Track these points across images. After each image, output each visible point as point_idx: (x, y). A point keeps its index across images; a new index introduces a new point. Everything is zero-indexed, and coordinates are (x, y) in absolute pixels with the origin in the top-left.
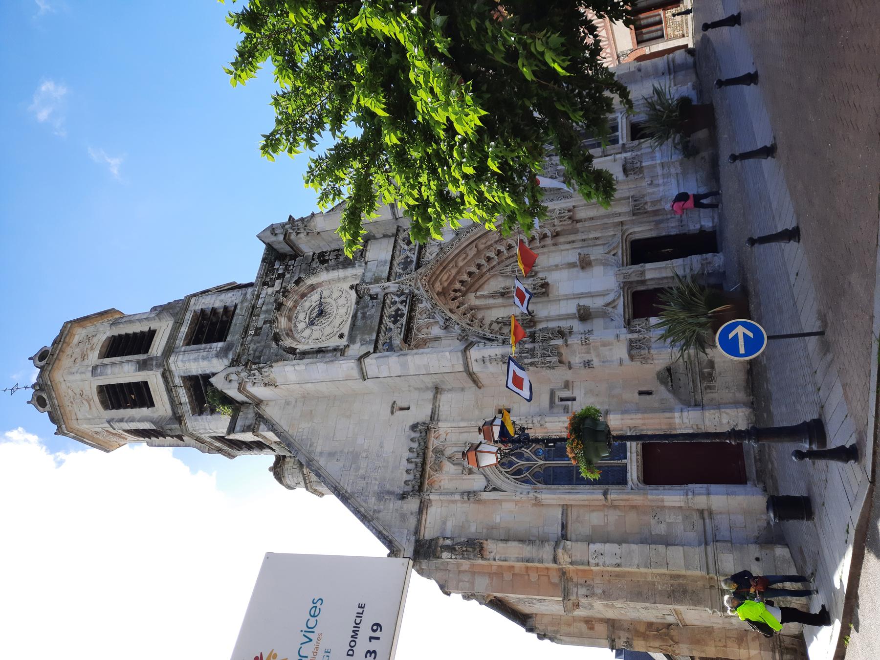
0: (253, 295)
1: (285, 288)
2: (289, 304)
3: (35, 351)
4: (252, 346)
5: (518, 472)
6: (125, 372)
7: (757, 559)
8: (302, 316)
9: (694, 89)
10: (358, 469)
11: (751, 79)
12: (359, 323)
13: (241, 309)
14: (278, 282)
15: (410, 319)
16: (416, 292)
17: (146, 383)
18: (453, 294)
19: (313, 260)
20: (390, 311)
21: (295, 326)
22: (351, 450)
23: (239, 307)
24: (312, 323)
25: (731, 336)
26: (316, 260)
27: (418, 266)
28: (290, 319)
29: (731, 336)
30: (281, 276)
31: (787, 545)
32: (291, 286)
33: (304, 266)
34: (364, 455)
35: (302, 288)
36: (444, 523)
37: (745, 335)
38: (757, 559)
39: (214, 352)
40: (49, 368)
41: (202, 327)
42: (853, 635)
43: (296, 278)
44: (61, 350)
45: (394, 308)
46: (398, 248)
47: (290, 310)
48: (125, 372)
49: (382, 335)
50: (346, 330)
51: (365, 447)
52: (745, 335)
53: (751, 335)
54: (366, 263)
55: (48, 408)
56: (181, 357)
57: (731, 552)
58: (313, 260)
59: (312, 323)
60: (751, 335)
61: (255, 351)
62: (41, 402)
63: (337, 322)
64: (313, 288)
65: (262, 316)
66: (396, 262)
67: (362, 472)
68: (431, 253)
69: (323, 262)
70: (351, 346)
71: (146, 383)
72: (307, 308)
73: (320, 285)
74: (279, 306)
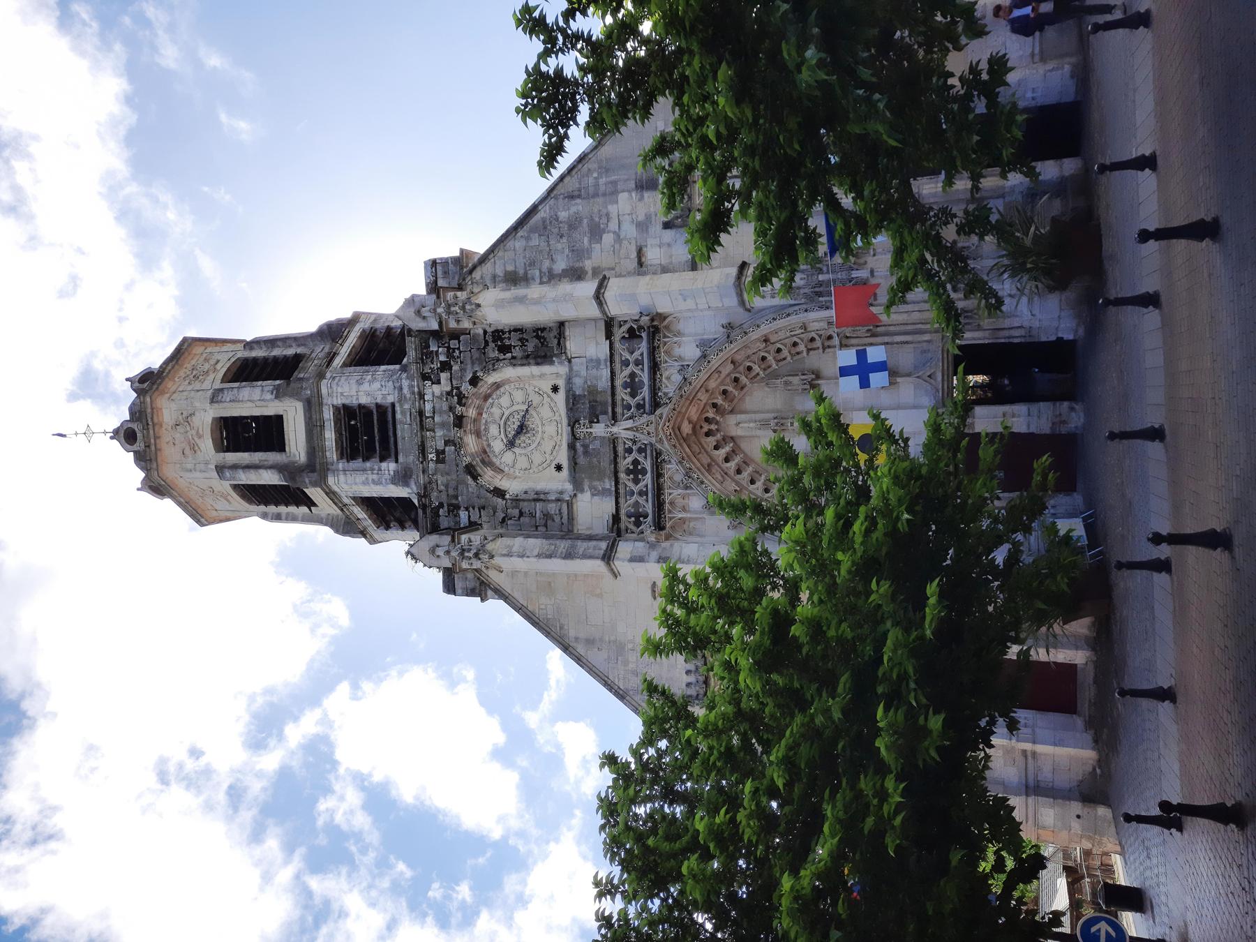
0: (413, 393)
1: (458, 388)
2: (471, 413)
3: (137, 369)
4: (441, 479)
6: (255, 401)
7: (1078, 817)
8: (494, 430)
9: (1072, 77)
10: (626, 663)
11: (1165, 695)
12: (582, 460)
13: (403, 413)
14: (444, 376)
15: (658, 475)
16: (659, 446)
17: (279, 419)
18: (706, 427)
19: (487, 343)
20: (626, 462)
21: (489, 445)
22: (612, 638)
23: (398, 408)
24: (511, 444)
25: (1093, 930)
26: (492, 345)
27: (656, 405)
28: (478, 434)
29: (1093, 930)
30: (445, 367)
31: (1109, 806)
32: (466, 388)
33: (476, 355)
34: (630, 646)
35: (483, 388)
37: (1107, 933)
38: (1078, 817)
39: (387, 476)
40: (154, 466)
41: (353, 431)
42: (1156, 829)
43: (469, 376)
44: (156, 438)
45: (630, 459)
47: (475, 420)
48: (255, 401)
49: (622, 500)
50: (563, 457)
51: (630, 637)
52: (1107, 933)
53: (1113, 934)
54: (570, 361)
55: (140, 445)
56: (342, 477)
57: (1052, 807)
58: (487, 343)
59: (511, 444)
60: (1113, 934)
61: (447, 486)
62: (127, 436)
63: (547, 446)
64: (497, 386)
65: (439, 433)
66: (618, 383)
67: (631, 666)
68: (671, 380)
69: (504, 349)
70: (579, 495)
71: (279, 419)
72: (497, 417)
73: (507, 381)
74: (459, 421)
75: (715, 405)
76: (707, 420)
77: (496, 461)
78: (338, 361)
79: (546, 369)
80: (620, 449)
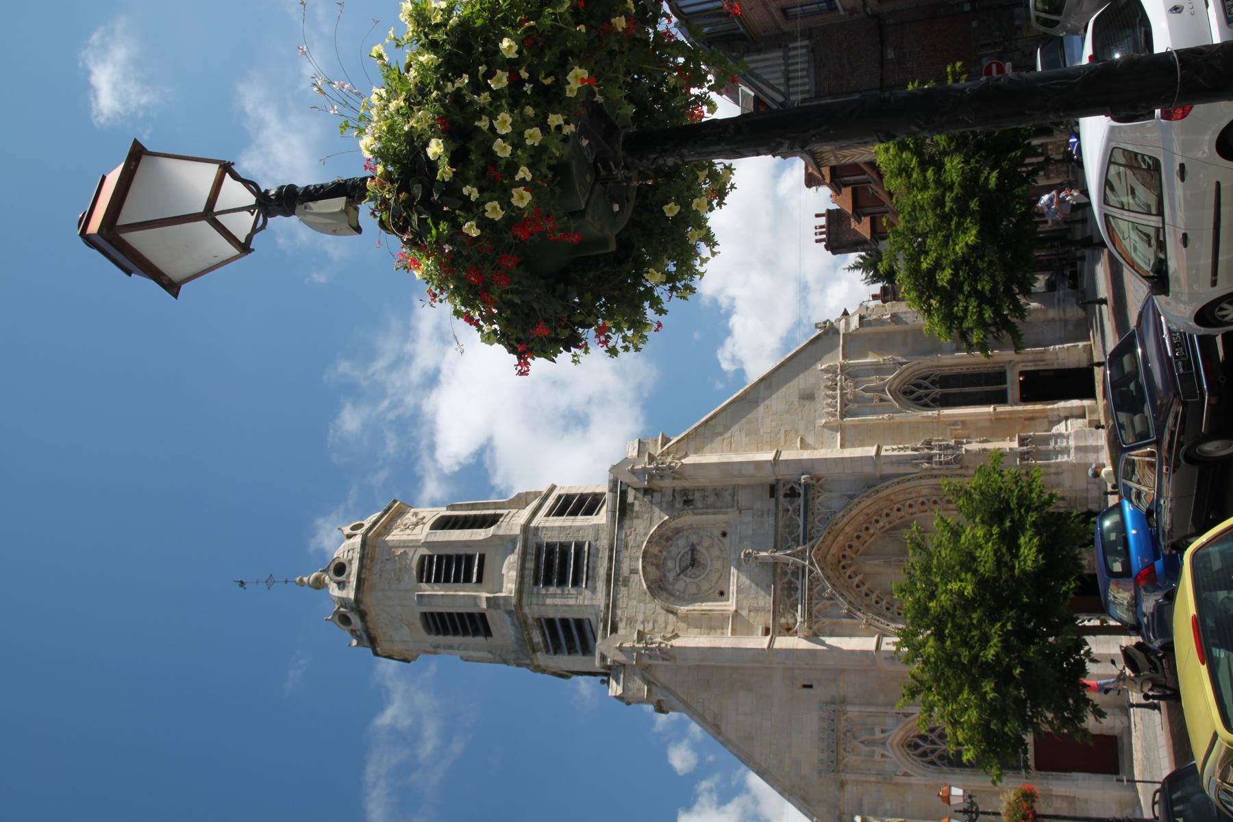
5: (919, 398)
36: (861, 800)
46: (780, 508)
75: (850, 547)
76: (844, 556)
77: (670, 587)
78: (545, 509)
79: (720, 517)
80: (779, 571)
